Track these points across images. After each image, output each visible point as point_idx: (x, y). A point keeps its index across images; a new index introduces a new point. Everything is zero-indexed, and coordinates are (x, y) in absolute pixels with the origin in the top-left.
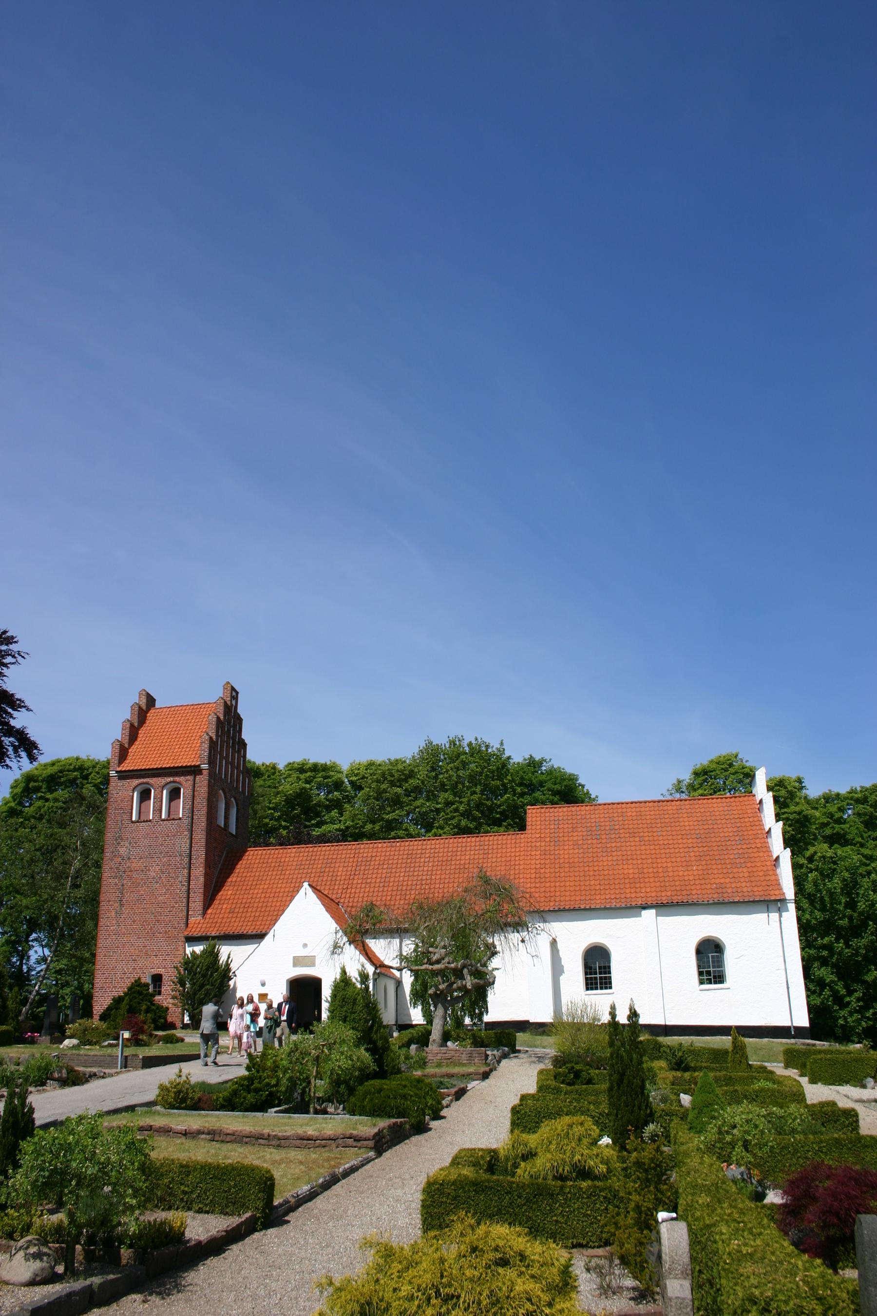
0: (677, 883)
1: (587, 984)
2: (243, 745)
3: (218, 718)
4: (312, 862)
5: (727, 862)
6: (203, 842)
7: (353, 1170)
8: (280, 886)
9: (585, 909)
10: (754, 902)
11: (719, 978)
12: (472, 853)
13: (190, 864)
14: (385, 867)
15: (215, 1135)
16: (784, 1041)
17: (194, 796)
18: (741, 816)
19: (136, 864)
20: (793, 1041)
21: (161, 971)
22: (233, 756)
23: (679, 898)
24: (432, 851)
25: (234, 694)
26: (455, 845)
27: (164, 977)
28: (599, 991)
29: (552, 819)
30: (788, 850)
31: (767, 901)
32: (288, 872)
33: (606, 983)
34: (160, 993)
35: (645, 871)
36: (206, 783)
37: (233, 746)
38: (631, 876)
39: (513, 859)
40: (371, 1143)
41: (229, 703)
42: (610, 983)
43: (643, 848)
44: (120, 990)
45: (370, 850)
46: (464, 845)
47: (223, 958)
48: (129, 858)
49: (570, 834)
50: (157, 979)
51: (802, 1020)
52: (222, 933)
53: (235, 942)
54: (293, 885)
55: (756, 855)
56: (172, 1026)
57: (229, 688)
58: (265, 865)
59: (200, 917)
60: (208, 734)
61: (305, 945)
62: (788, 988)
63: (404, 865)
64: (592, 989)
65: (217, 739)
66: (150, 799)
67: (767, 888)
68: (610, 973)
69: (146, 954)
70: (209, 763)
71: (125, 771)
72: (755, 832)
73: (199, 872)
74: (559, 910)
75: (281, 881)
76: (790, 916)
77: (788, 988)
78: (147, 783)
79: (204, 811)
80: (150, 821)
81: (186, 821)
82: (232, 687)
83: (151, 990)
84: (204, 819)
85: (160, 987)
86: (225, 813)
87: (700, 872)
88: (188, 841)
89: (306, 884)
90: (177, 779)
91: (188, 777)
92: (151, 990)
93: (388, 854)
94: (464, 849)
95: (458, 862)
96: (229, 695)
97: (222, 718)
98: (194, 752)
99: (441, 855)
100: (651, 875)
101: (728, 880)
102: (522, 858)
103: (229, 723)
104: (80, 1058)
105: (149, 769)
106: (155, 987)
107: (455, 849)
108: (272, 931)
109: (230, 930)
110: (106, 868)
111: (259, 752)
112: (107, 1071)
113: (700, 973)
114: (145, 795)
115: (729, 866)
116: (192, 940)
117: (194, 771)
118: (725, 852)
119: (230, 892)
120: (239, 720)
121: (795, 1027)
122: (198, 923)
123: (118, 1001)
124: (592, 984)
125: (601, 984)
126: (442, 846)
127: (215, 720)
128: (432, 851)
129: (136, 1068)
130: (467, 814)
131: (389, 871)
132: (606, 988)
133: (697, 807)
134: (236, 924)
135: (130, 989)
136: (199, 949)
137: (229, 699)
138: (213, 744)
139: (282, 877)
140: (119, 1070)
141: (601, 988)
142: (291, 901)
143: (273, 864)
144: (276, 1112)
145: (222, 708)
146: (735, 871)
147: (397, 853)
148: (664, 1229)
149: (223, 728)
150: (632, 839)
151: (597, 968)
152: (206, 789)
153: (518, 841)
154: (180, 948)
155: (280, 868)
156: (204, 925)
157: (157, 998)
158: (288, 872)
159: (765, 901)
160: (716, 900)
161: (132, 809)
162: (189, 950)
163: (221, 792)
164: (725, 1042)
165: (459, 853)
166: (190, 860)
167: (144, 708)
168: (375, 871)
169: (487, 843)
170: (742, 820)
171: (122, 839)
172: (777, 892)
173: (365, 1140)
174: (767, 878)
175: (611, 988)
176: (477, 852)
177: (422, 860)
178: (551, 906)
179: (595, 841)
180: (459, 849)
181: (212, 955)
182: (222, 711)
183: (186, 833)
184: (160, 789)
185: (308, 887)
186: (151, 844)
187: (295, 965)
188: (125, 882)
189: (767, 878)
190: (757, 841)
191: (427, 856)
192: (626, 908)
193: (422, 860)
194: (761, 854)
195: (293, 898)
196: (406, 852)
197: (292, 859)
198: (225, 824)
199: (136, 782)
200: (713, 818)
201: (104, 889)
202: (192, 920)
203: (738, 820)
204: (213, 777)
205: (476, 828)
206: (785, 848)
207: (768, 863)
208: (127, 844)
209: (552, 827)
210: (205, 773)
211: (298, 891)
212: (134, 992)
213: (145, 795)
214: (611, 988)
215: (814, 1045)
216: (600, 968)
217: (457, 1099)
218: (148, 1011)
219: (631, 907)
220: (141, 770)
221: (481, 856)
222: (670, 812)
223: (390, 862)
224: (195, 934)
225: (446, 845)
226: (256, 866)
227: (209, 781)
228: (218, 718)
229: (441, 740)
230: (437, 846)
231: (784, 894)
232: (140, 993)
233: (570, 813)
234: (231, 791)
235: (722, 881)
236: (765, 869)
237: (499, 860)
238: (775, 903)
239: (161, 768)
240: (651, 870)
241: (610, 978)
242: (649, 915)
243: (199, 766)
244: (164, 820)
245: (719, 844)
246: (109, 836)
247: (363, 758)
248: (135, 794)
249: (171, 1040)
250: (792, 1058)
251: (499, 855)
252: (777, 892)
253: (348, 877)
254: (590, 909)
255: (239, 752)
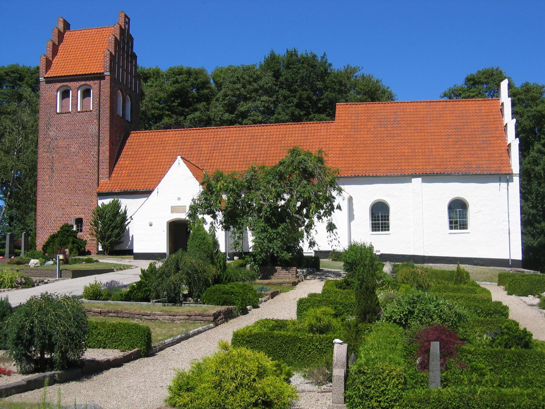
0: (438, 160)
1: (373, 227)
2: (134, 57)
3: (116, 38)
4: (184, 141)
5: (475, 146)
6: (108, 127)
7: (199, 332)
8: (162, 157)
9: (373, 176)
10: (490, 174)
11: (464, 226)
12: (297, 135)
13: (99, 142)
14: (235, 144)
15: (117, 313)
16: (498, 268)
17: (100, 94)
18: (487, 114)
19: (61, 143)
20: (510, 269)
21: (82, 216)
22: (127, 67)
23: (439, 170)
24: (269, 134)
25: (127, 20)
26: (285, 130)
27: (84, 220)
28: (380, 232)
29: (353, 112)
30: (518, 139)
31: (500, 174)
32: (167, 148)
33: (385, 227)
34: (81, 231)
35: (417, 151)
36: (108, 85)
37: (127, 58)
38: (406, 154)
39: (325, 140)
40: (212, 318)
41: (123, 27)
42: (388, 227)
43: (416, 135)
44: (55, 229)
45: (225, 133)
46: (291, 130)
47: (123, 208)
48: (56, 139)
49: (366, 124)
50: (79, 221)
51: (517, 255)
52: (122, 191)
53: (132, 196)
54: (171, 157)
55: (495, 142)
56: (89, 253)
57: (123, 16)
58: (151, 143)
59: (107, 179)
60: (108, 50)
61: (179, 199)
62: (509, 234)
63: (248, 144)
64: (376, 231)
65: (115, 53)
66: (69, 97)
67: (501, 165)
68: (388, 220)
69: (71, 205)
70: (110, 71)
71: (51, 77)
72: (496, 126)
73: (105, 148)
74: (355, 176)
75: (162, 154)
76: (515, 185)
77: (509, 234)
78: (67, 86)
79: (108, 105)
80: (70, 113)
81: (95, 113)
82: (125, 15)
83: (75, 229)
84: (108, 111)
85: (81, 226)
86: (123, 103)
87: (455, 153)
88: (97, 127)
89: (179, 157)
90: (88, 83)
91: (96, 81)
92: (75, 229)
93: (237, 135)
94: (291, 133)
95: (286, 142)
96: (123, 21)
97: (118, 38)
98: (100, 63)
99: (274, 136)
100: (420, 154)
101: (473, 159)
102: (331, 140)
103: (124, 45)
104: (32, 271)
105: (67, 76)
106: (78, 227)
107: (284, 133)
108: (156, 189)
109: (132, 187)
110: (40, 145)
111: (146, 61)
112: (50, 279)
113: (451, 223)
114: (65, 94)
115: (475, 149)
116: (101, 195)
117: (99, 77)
118: (474, 140)
119: (127, 162)
120: (131, 39)
121: (512, 260)
122: (106, 184)
123: (53, 237)
124: (375, 227)
125: (382, 227)
126: (275, 130)
127: (113, 40)
128: (269, 134)
129: (67, 277)
130: (299, 106)
131: (238, 147)
132: (385, 230)
133: (457, 106)
134: (132, 184)
135: (61, 228)
136: (107, 201)
137: (123, 24)
138: (112, 58)
139: (163, 151)
140: (57, 278)
141: (382, 230)
142: (170, 168)
143: (157, 142)
144: (155, 302)
145: (118, 31)
146: (479, 152)
147: (243, 135)
148: (336, 346)
149: (119, 45)
150: (409, 128)
151: (380, 216)
152: (109, 90)
153: (329, 128)
154: (94, 200)
155: (162, 145)
156: (110, 185)
157: (79, 234)
158: (167, 148)
159: (498, 174)
160: (464, 173)
161: (57, 105)
162: (100, 202)
163: (119, 91)
164: (453, 267)
165: (287, 136)
166: (99, 139)
167: (62, 31)
168: (228, 147)
169: (307, 129)
170: (488, 117)
171: (51, 126)
172: (507, 169)
173: (208, 316)
174: (501, 158)
175: (388, 230)
176: (300, 135)
177: (261, 140)
178: (349, 173)
179: (382, 129)
180: (287, 133)
181: (116, 206)
182: (118, 33)
183: (95, 121)
184: (76, 90)
185: (181, 160)
186: (71, 122)
187: (172, 212)
188: (54, 155)
189: (501, 158)
190: (497, 132)
191: (265, 137)
192: (401, 176)
193: (261, 140)
194: (499, 142)
195: (171, 165)
196: (250, 134)
197: (170, 139)
198: (123, 115)
199: (59, 85)
200: (468, 115)
201: (40, 160)
202: (102, 181)
203: (485, 117)
204: (113, 80)
205: (305, 115)
206: (516, 138)
207: (503, 148)
208: (54, 129)
209: (353, 118)
210: (108, 78)
211: (175, 161)
212: (64, 230)
213: (65, 94)
214: (388, 230)
215: (523, 272)
216: (382, 217)
217: (272, 298)
218: (73, 242)
219: (405, 176)
220: (62, 76)
221: (303, 138)
222: (437, 110)
223: (239, 141)
224: (104, 191)
225: (279, 130)
226: (145, 143)
227: (111, 84)
228: (116, 38)
229: (281, 52)
230: (272, 131)
231: (512, 170)
232: (67, 231)
233: (366, 109)
234: (126, 91)
235: (469, 159)
236: (500, 152)
237: (315, 141)
238: (504, 177)
239: (76, 75)
240: (420, 151)
241: (388, 224)
242: (417, 181)
243: (103, 73)
244: (80, 112)
245: (470, 133)
246: (42, 124)
247: (225, 64)
248: (59, 93)
249: (89, 261)
250: (502, 280)
251: (315, 137)
252: (507, 169)
253: (209, 152)
254: (376, 176)
255: (132, 62)
